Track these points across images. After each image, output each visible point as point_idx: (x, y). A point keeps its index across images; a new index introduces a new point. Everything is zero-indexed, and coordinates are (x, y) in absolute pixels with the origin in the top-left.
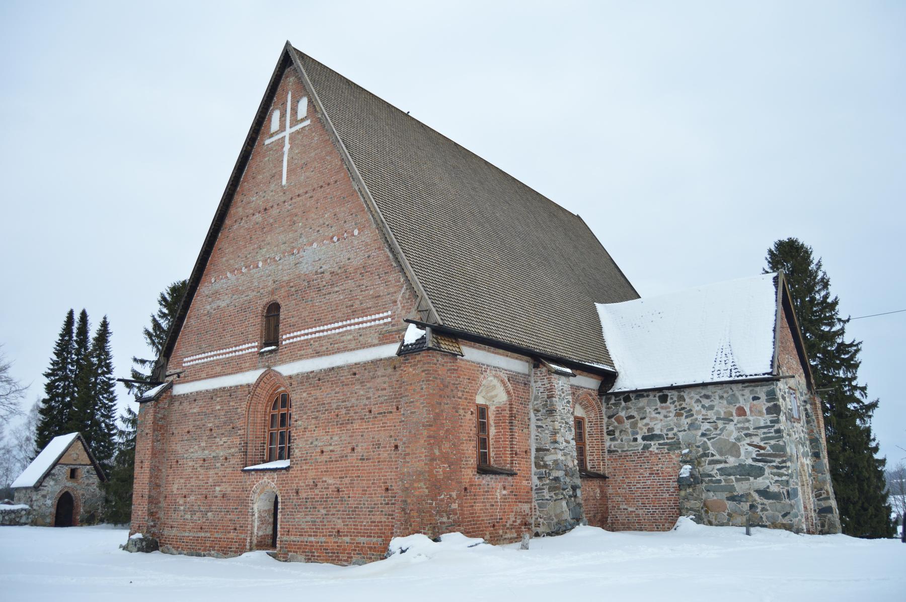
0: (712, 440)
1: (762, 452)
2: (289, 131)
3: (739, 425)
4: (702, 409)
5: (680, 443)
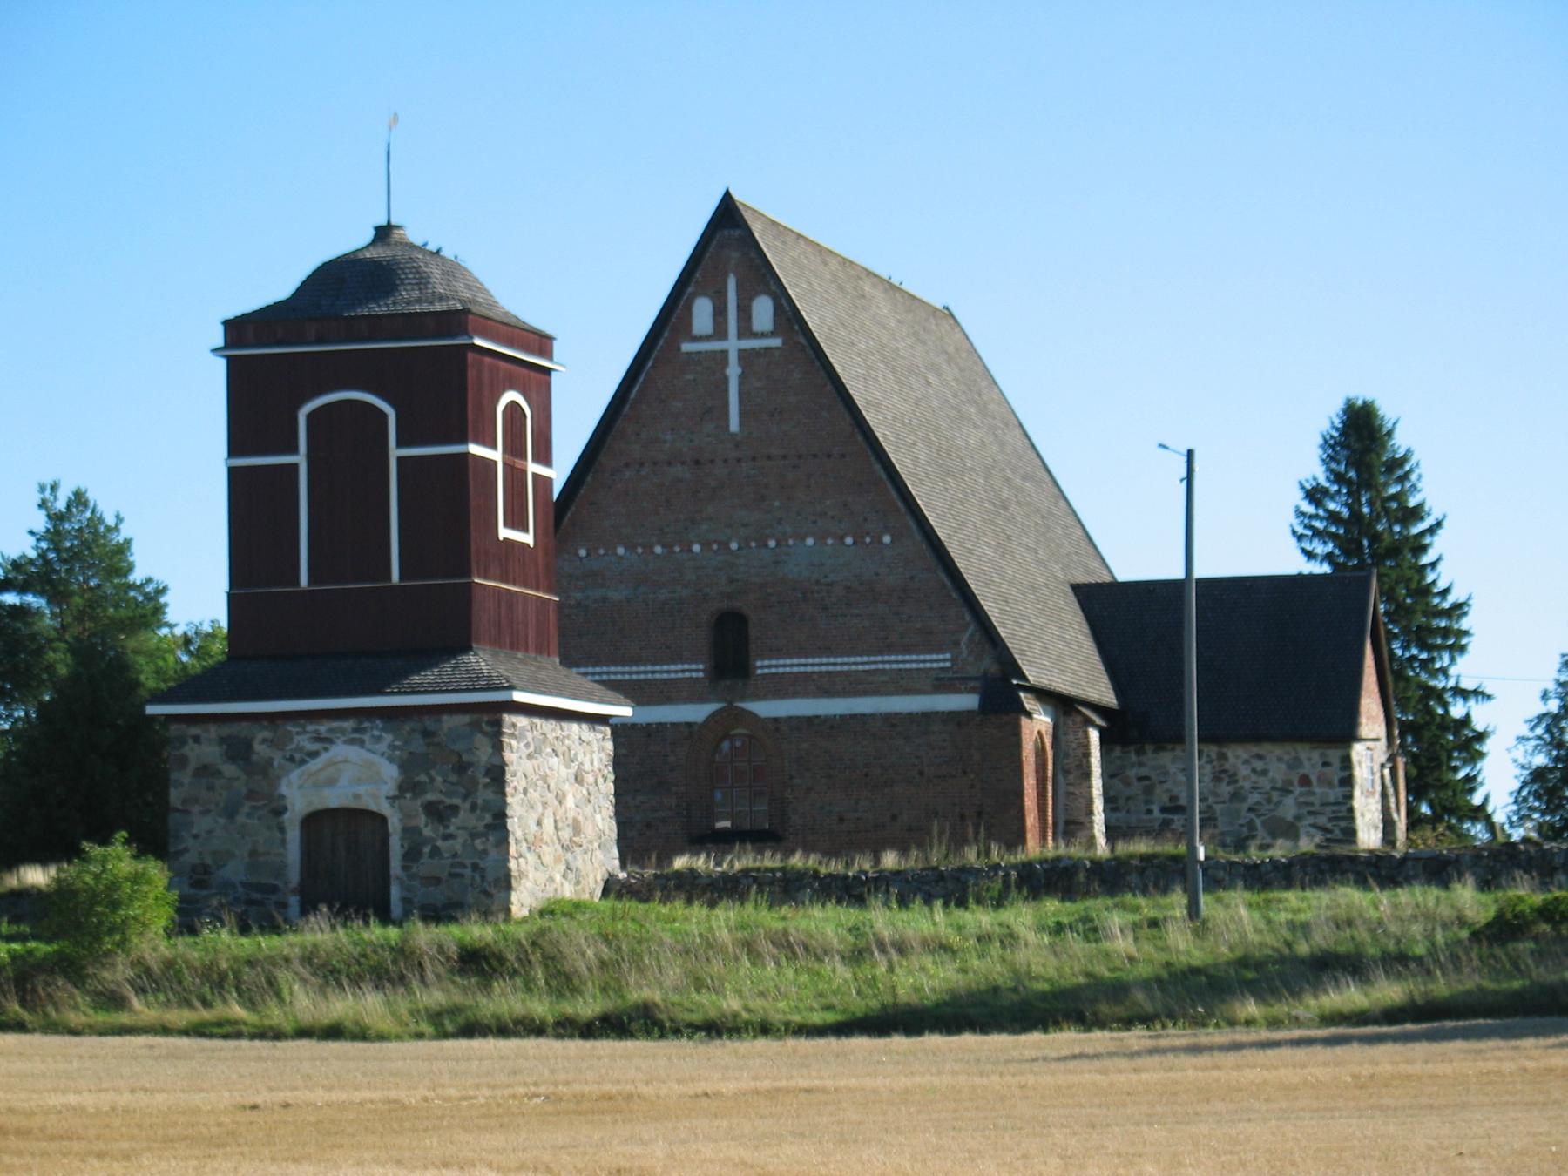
0: (1263, 818)
1: (1329, 836)
2: (733, 345)
3: (1302, 799)
4: (1252, 775)
5: (1215, 819)
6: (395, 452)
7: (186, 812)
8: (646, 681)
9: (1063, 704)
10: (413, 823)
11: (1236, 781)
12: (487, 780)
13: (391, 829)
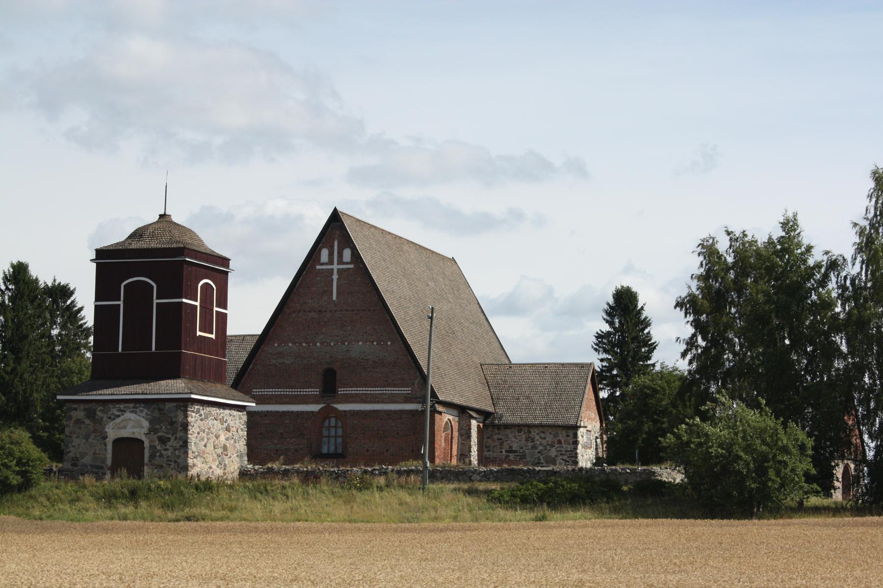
5: (526, 456)
6: (155, 301)
7: (71, 437)
8: (297, 395)
9: (462, 411)
10: (153, 444)
11: (534, 441)
12: (181, 428)
13: (145, 446)
